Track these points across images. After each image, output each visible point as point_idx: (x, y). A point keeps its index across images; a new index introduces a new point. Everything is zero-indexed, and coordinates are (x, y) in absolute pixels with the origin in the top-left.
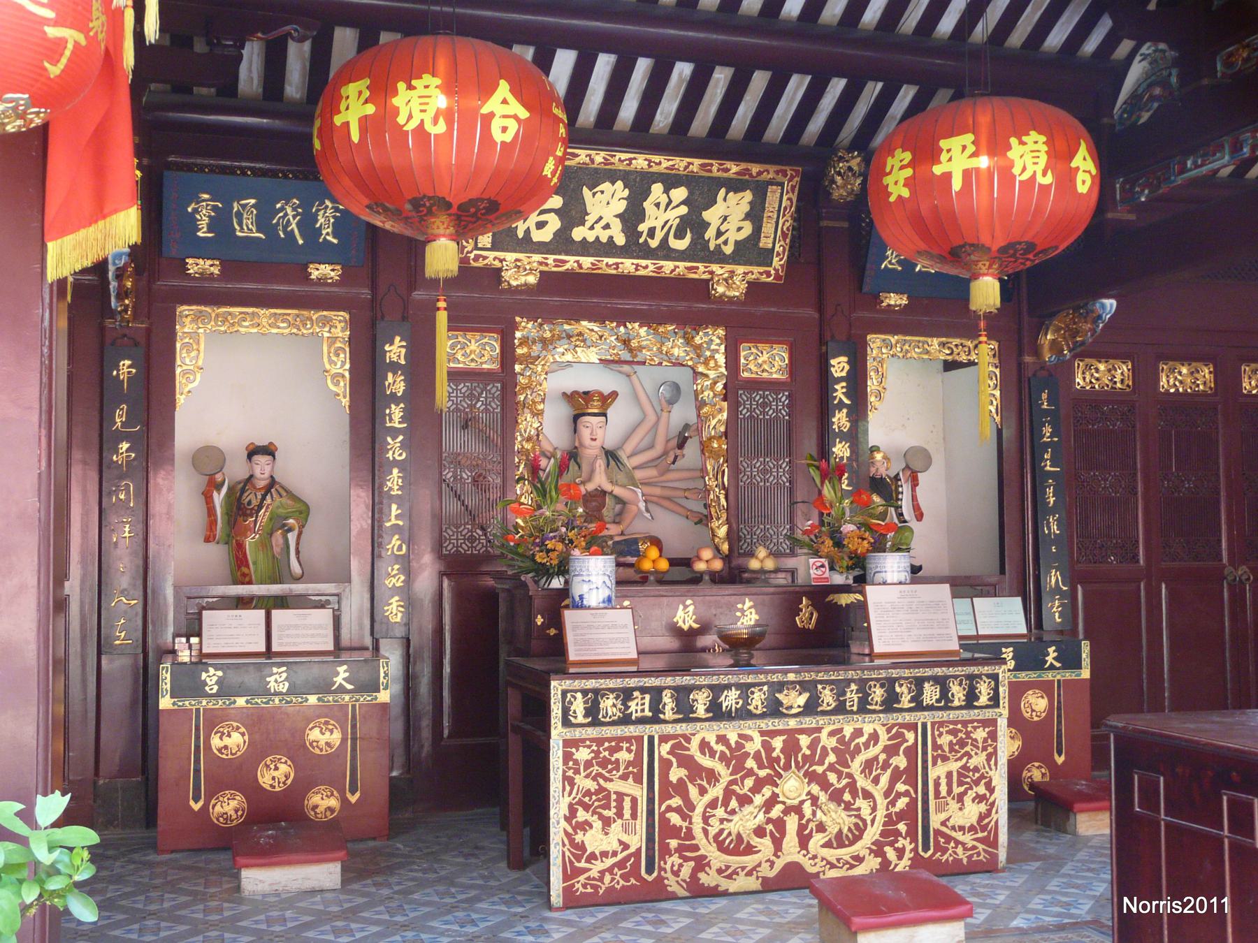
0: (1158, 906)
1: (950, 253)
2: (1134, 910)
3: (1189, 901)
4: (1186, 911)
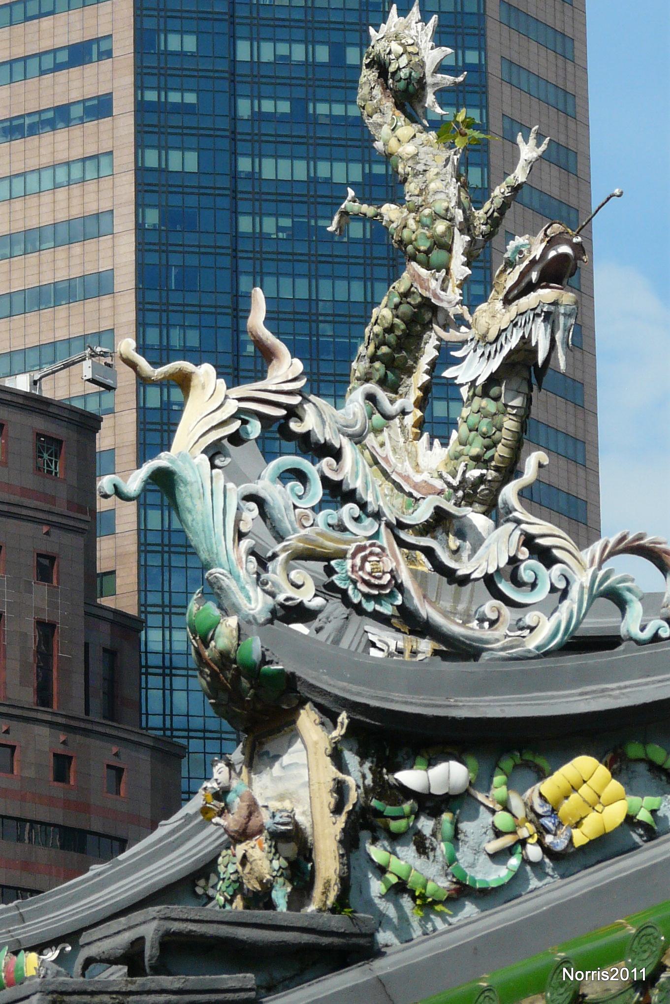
0: (590, 975)
1: (461, 444)
2: (572, 978)
3: (615, 971)
4: (612, 979)
